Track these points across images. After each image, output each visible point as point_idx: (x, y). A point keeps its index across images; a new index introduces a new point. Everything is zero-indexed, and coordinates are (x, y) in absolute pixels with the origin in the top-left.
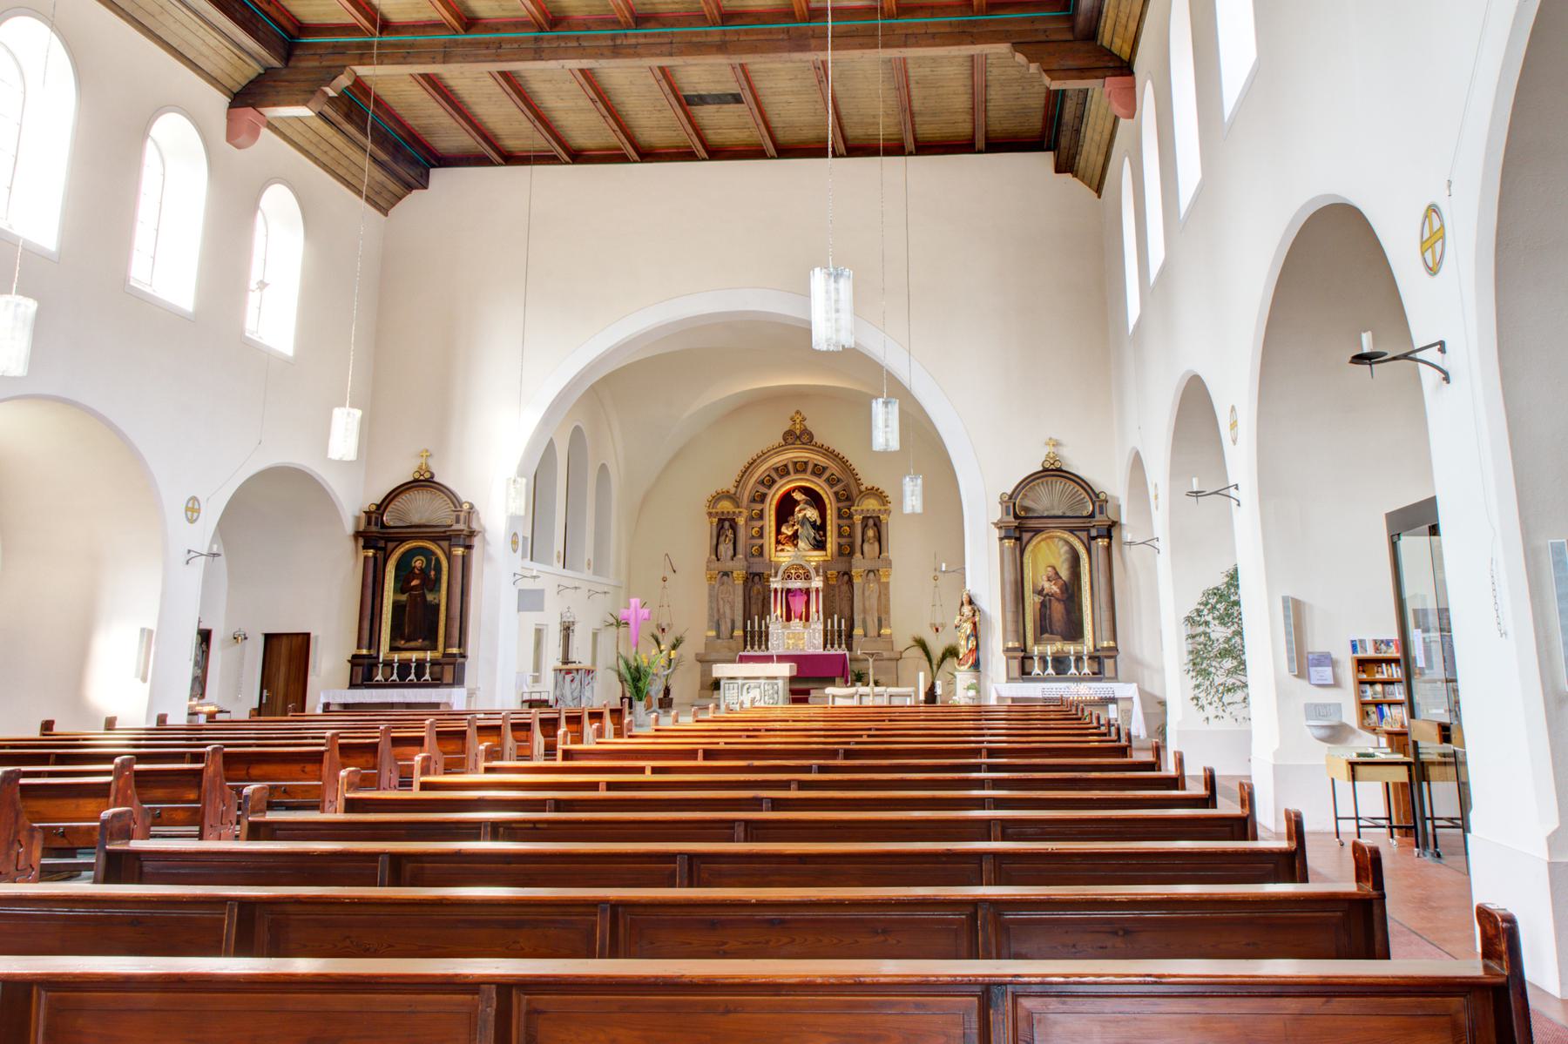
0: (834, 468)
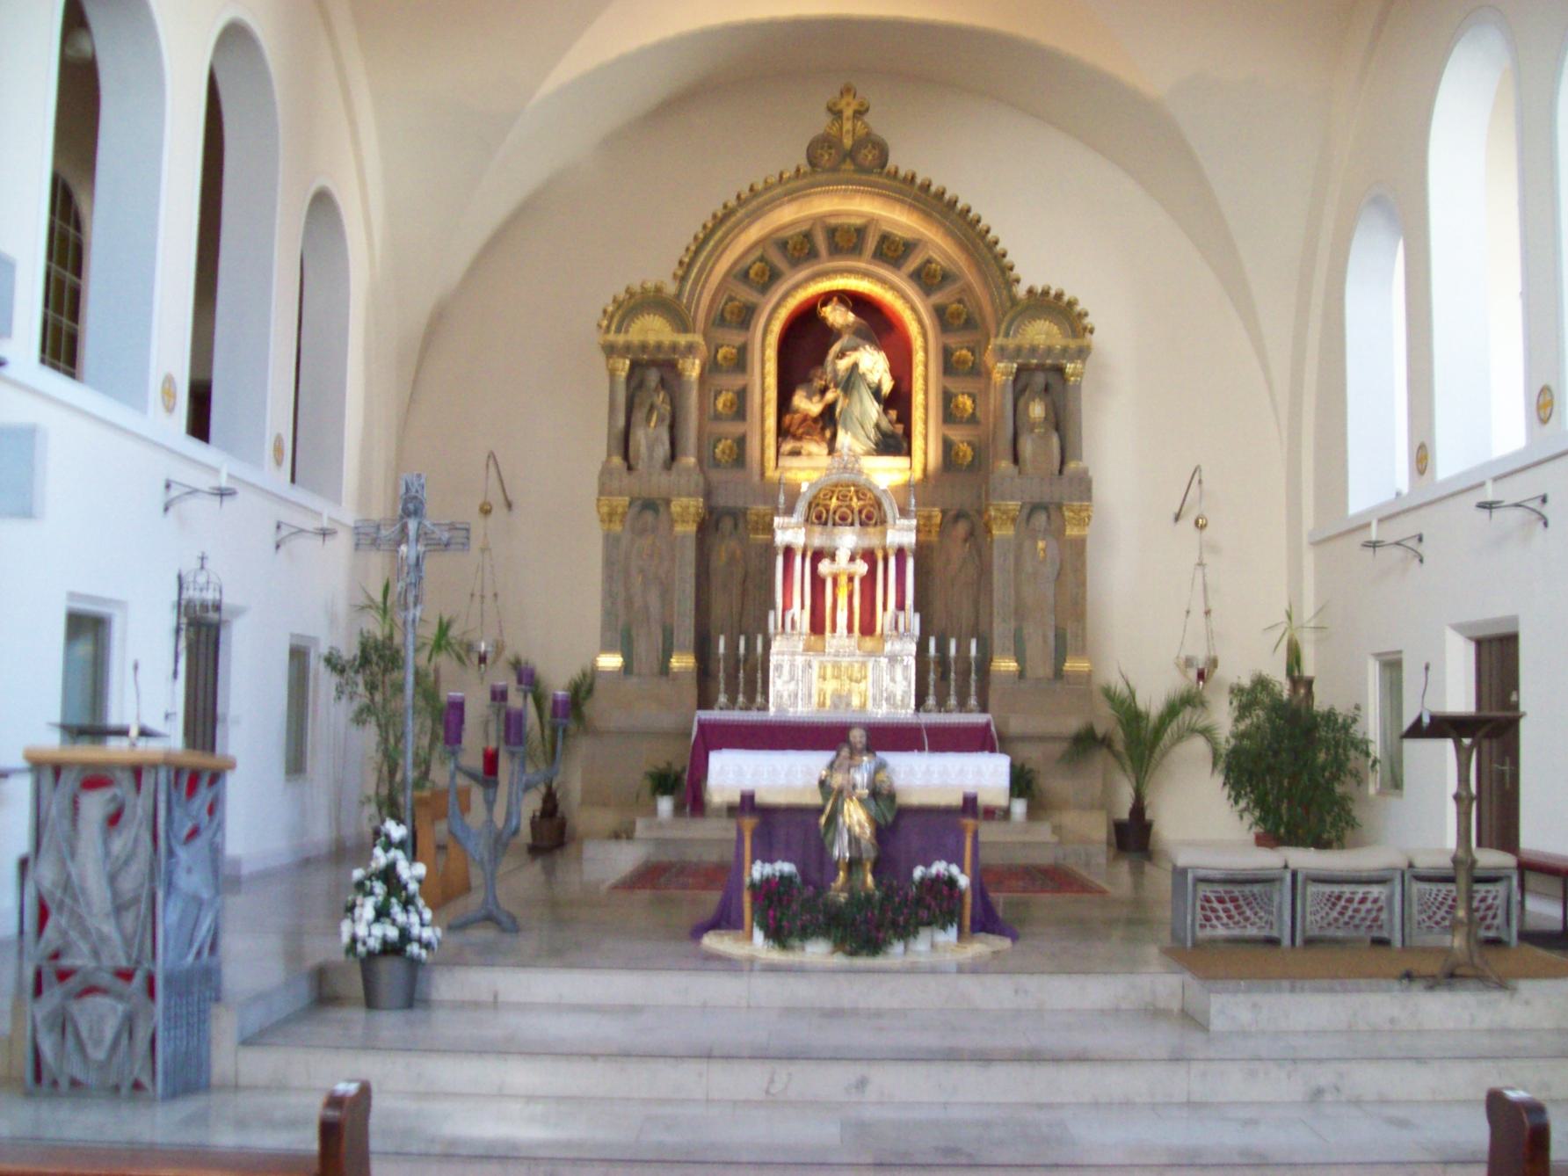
0: (938, 244)
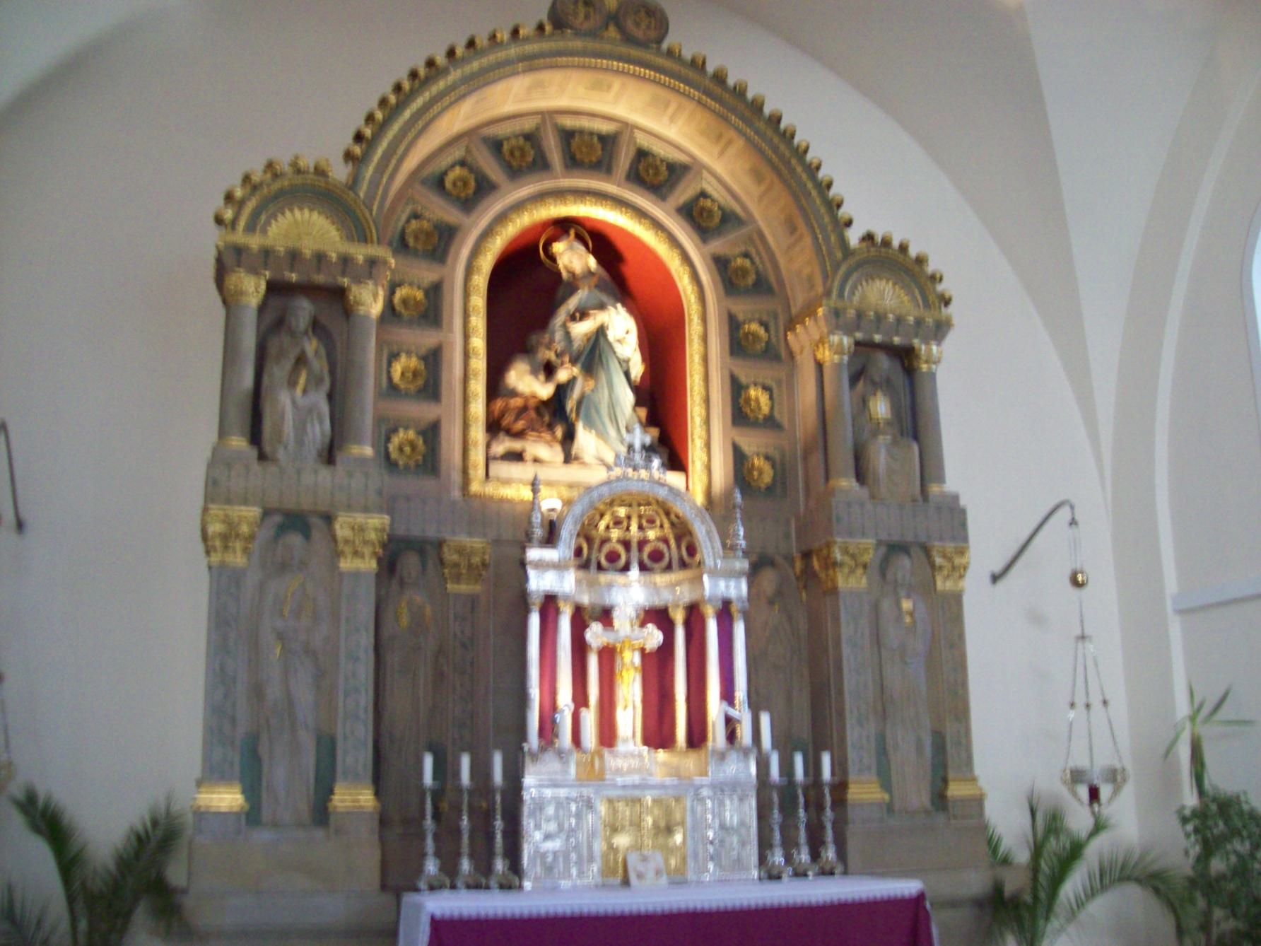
0: (723, 168)
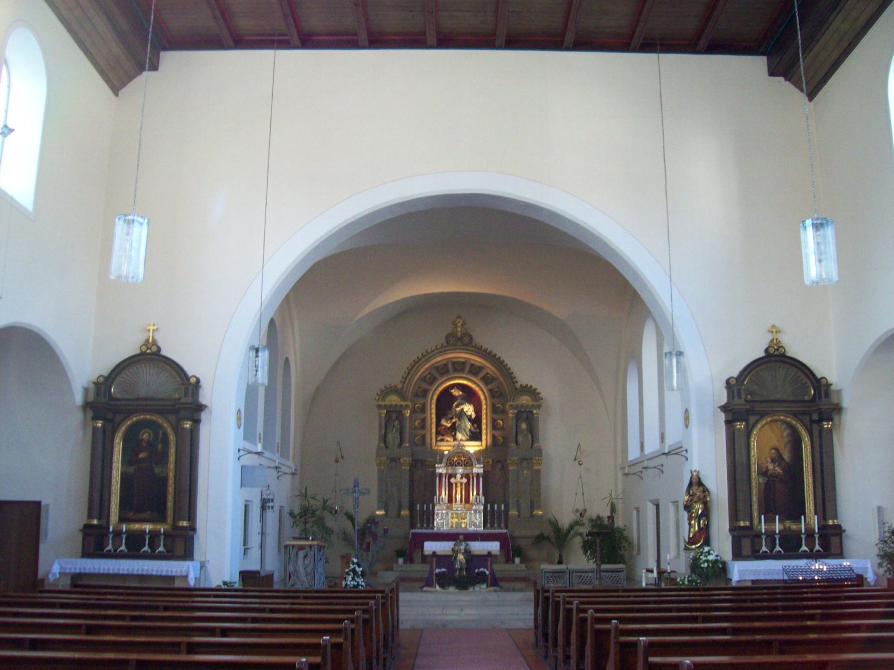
0: (490, 368)
